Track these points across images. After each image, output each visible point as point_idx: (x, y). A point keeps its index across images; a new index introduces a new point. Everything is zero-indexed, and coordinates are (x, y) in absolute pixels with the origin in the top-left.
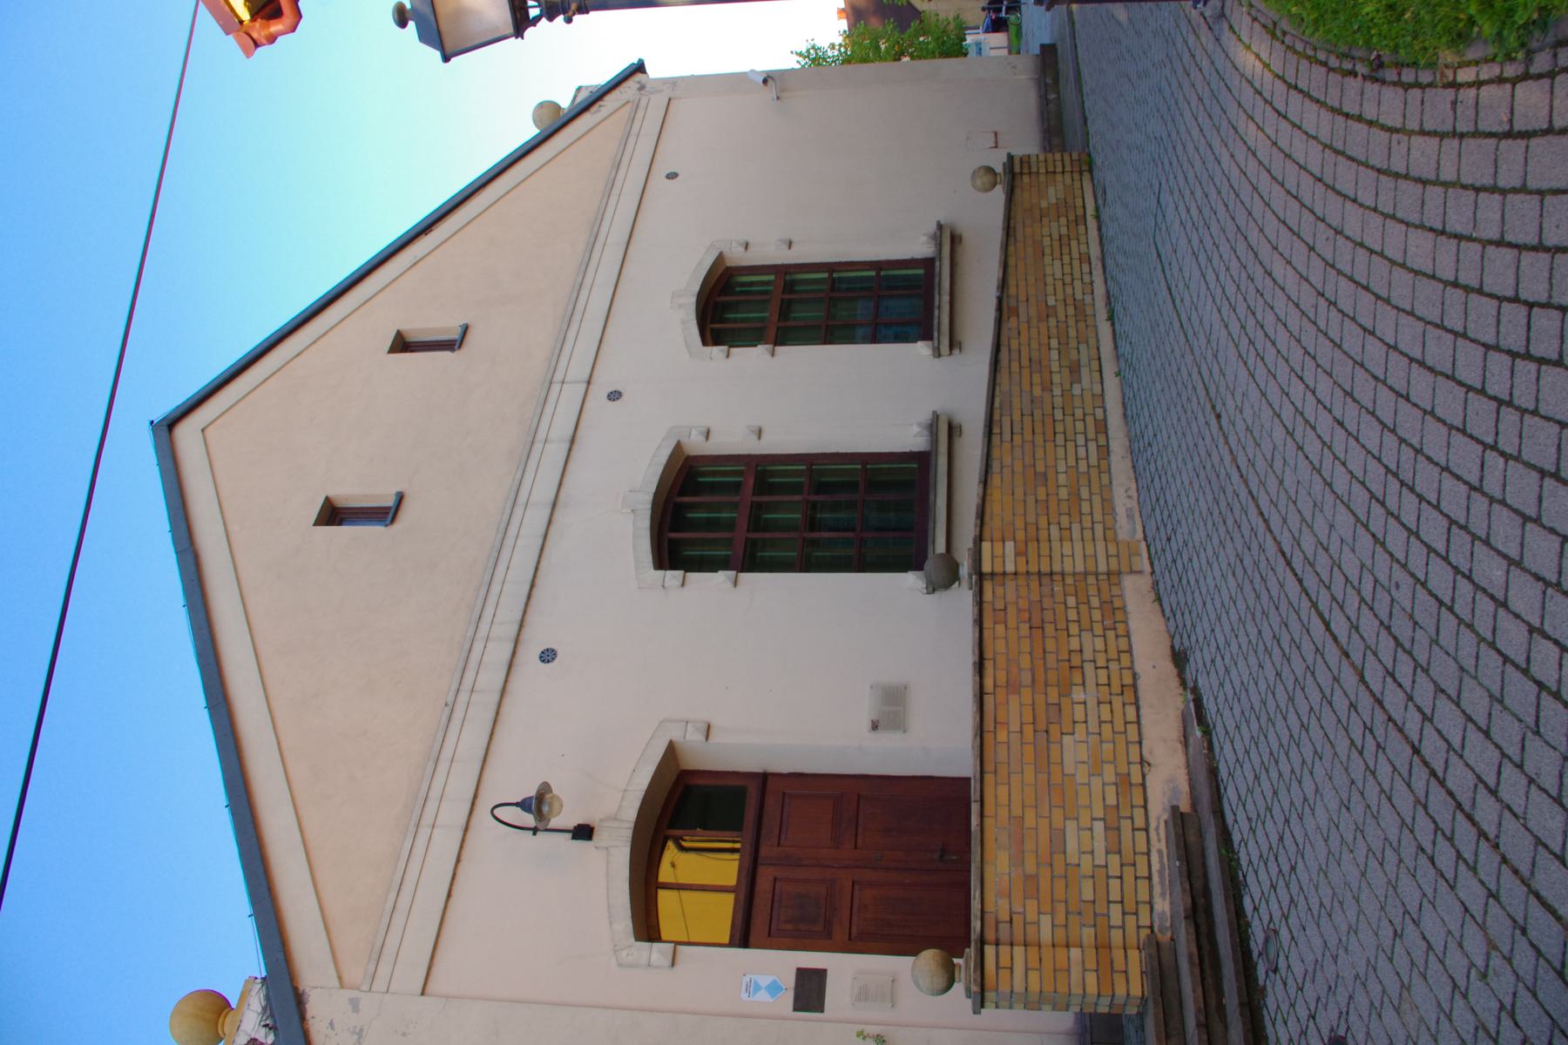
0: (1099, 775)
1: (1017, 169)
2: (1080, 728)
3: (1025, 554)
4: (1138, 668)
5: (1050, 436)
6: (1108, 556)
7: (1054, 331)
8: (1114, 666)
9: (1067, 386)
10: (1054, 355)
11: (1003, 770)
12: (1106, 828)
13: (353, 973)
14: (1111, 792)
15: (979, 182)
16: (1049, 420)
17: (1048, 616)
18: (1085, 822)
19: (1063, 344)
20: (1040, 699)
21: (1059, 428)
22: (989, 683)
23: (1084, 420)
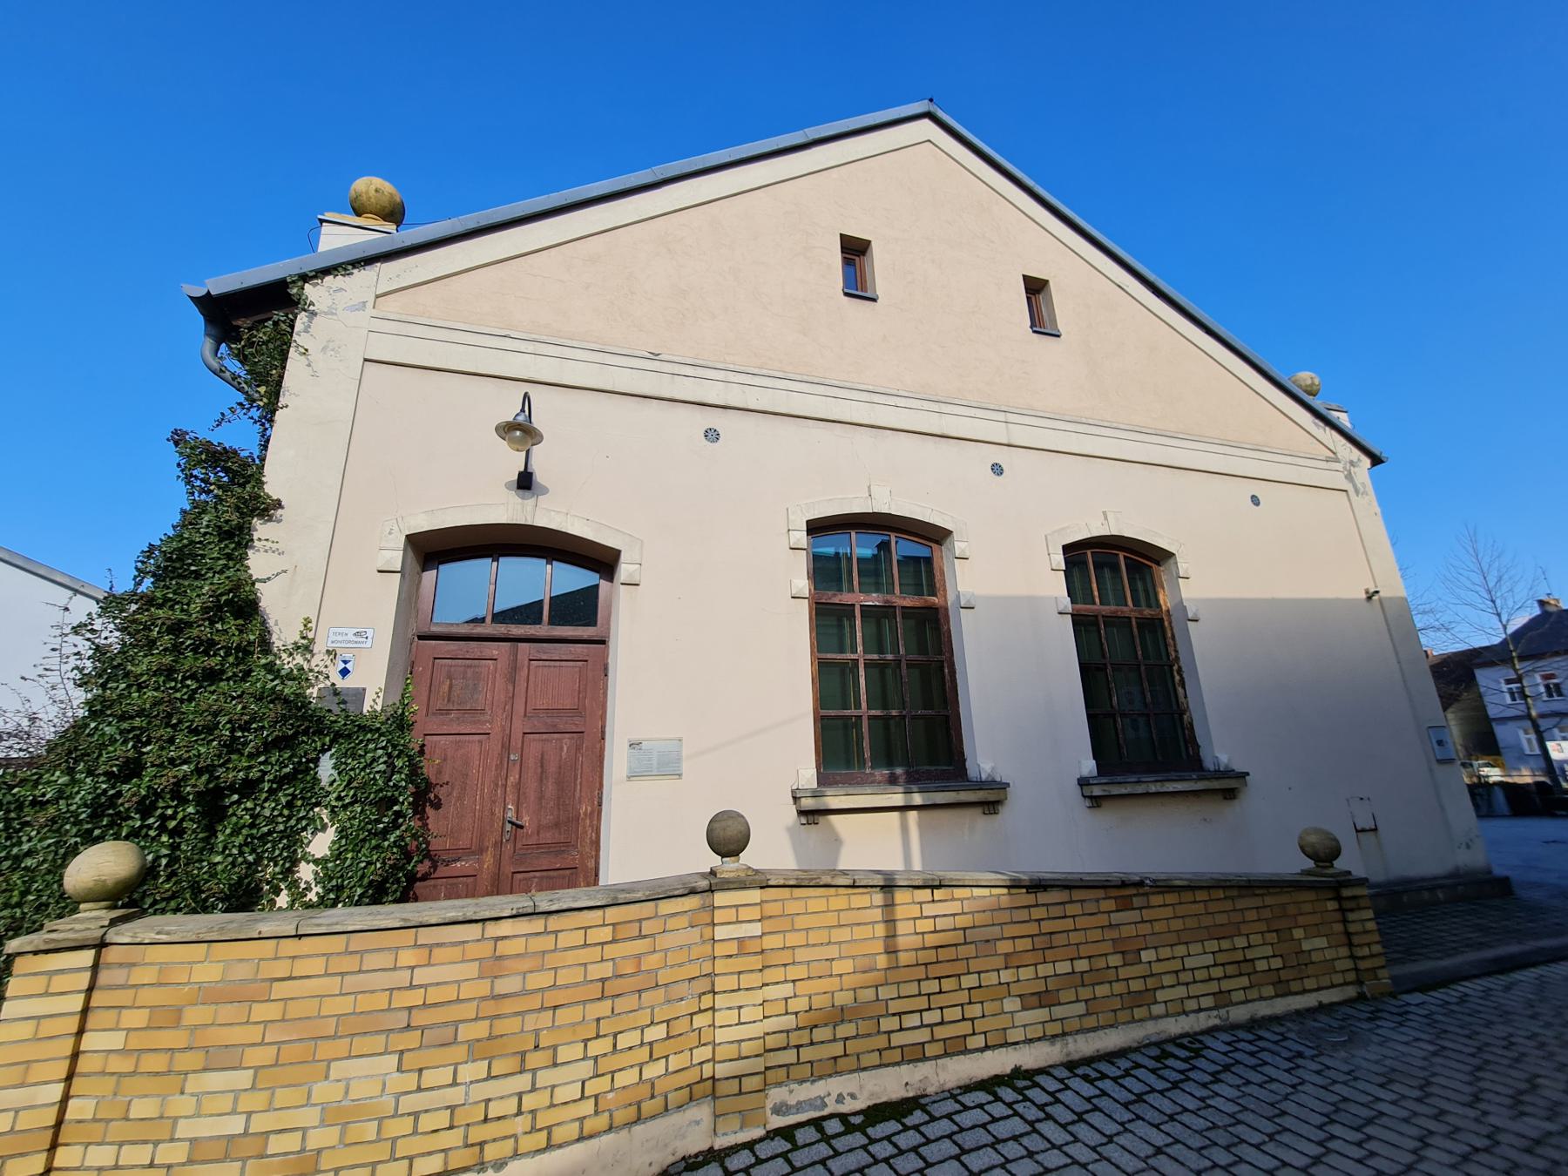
0: (322, 1120)
1: (1346, 893)
2: (411, 1081)
3: (741, 953)
4: (514, 1166)
5: (935, 971)
6: (740, 1077)
7: (1101, 963)
8: (522, 1123)
9: (1015, 989)
10: (1063, 967)
11: (349, 963)
12: (231, 1138)
13: (391, 306)
14: (291, 1143)
15: (1313, 839)
16: (960, 967)
17: (622, 1004)
18: (247, 1103)
19: (1080, 979)
20: (469, 1010)
21: (948, 984)
22: (505, 928)
23: (964, 1019)
